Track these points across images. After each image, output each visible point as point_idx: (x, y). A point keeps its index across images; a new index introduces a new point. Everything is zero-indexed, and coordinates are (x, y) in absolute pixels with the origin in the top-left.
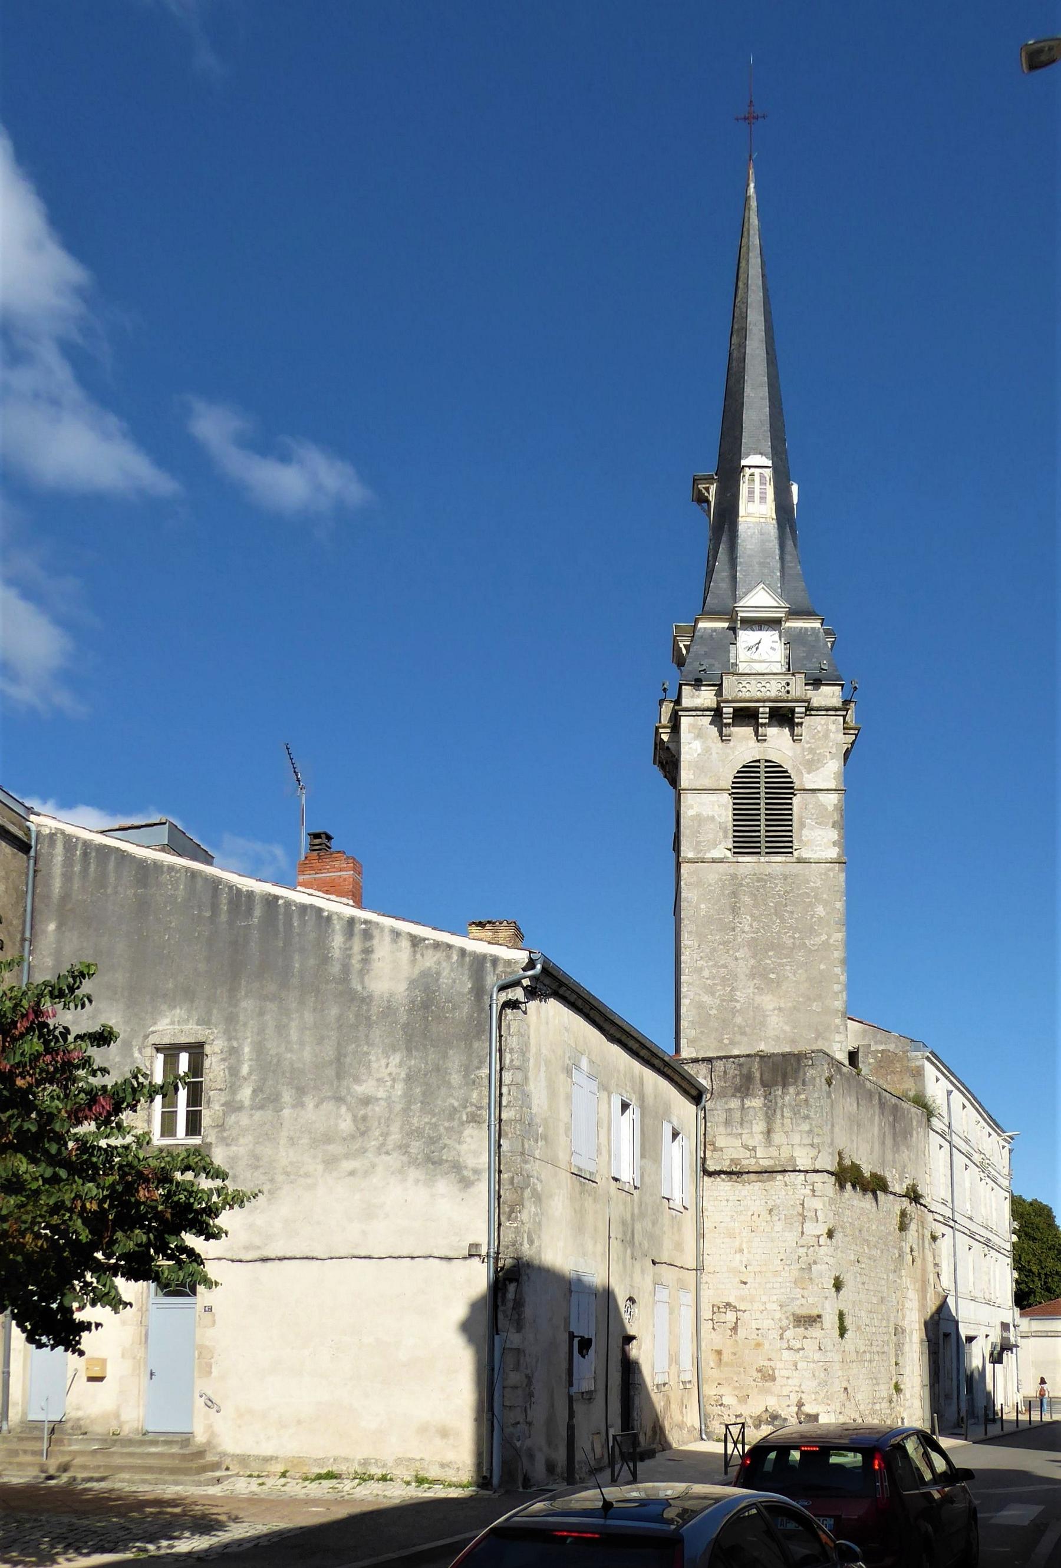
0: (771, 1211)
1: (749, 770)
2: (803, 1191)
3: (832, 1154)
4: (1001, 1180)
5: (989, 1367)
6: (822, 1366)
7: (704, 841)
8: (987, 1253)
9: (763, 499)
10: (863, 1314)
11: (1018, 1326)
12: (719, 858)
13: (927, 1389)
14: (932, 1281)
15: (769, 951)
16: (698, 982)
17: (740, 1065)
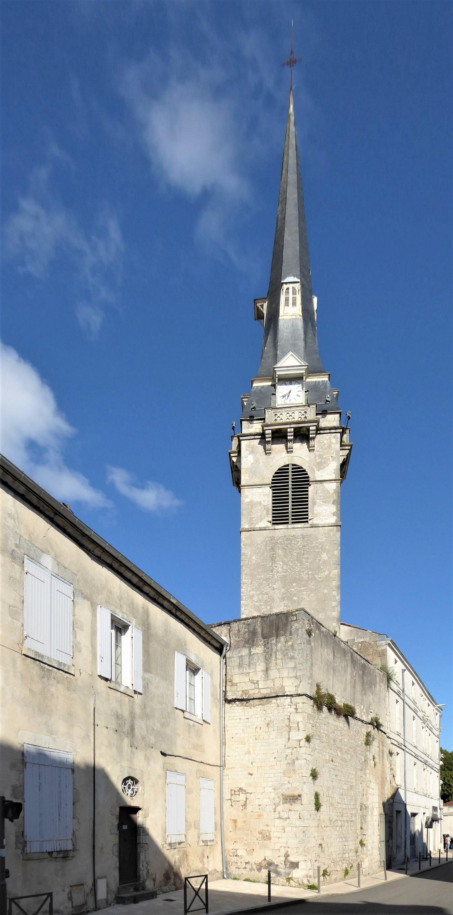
0: (268, 724)
1: (282, 471)
2: (289, 710)
3: (311, 685)
4: (434, 730)
5: (425, 830)
6: (301, 830)
7: (255, 518)
8: (426, 768)
9: (294, 304)
10: (336, 796)
11: (442, 809)
12: (263, 527)
13: (383, 845)
14: (388, 779)
15: (293, 583)
16: (251, 604)
17: (249, 625)
